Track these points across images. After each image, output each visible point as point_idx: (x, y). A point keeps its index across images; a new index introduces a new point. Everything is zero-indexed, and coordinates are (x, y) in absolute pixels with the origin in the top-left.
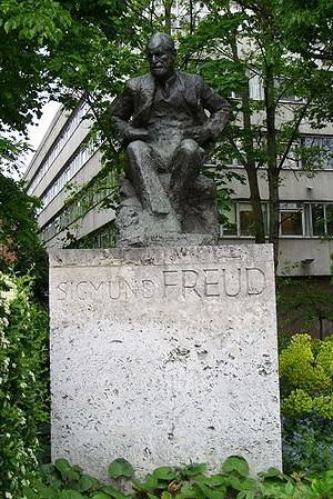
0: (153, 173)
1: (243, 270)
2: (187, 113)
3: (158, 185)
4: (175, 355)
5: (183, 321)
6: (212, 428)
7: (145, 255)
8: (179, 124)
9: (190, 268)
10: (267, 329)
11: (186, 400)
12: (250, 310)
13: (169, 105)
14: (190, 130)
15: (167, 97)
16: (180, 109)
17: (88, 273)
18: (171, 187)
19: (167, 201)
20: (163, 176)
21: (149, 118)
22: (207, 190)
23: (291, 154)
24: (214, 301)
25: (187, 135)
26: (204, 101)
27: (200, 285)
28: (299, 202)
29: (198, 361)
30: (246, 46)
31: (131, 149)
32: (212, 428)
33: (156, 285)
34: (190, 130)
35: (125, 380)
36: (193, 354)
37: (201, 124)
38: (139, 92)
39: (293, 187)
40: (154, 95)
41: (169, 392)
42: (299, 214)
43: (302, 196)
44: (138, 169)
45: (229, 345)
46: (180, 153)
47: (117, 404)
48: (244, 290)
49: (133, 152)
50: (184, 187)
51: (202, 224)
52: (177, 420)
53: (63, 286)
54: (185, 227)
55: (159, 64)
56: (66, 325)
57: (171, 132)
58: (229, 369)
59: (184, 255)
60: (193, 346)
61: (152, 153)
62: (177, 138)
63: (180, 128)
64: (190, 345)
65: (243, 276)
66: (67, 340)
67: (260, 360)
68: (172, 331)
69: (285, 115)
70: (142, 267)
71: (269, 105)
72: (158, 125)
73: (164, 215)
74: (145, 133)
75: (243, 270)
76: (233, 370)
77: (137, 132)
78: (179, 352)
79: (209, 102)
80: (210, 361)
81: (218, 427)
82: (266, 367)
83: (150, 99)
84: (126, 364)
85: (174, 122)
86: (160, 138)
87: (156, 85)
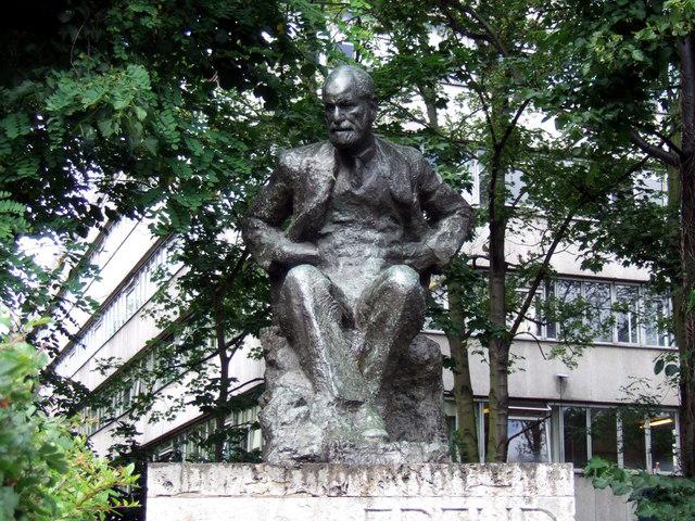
0: (334, 325)
1: (516, 511)
2: (393, 218)
8: (378, 236)
13: (361, 202)
14: (396, 248)
15: (358, 186)
16: (379, 209)
21: (323, 225)
22: (428, 362)
23: (532, 312)
25: (393, 259)
26: (424, 196)
30: (460, 108)
31: (293, 279)
34: (396, 248)
38: (305, 175)
39: (533, 373)
40: (333, 183)
43: (548, 390)
44: (306, 317)
46: (380, 293)
49: (297, 286)
50: (392, 356)
51: (417, 427)
54: (395, 434)
55: (345, 124)
57: (360, 253)
61: (334, 291)
62: (374, 263)
63: (380, 244)
69: (523, 243)
70: (324, 499)
71: (498, 219)
72: (339, 238)
79: (433, 199)
83: (324, 187)
85: (370, 234)
86: (342, 261)
87: (337, 162)
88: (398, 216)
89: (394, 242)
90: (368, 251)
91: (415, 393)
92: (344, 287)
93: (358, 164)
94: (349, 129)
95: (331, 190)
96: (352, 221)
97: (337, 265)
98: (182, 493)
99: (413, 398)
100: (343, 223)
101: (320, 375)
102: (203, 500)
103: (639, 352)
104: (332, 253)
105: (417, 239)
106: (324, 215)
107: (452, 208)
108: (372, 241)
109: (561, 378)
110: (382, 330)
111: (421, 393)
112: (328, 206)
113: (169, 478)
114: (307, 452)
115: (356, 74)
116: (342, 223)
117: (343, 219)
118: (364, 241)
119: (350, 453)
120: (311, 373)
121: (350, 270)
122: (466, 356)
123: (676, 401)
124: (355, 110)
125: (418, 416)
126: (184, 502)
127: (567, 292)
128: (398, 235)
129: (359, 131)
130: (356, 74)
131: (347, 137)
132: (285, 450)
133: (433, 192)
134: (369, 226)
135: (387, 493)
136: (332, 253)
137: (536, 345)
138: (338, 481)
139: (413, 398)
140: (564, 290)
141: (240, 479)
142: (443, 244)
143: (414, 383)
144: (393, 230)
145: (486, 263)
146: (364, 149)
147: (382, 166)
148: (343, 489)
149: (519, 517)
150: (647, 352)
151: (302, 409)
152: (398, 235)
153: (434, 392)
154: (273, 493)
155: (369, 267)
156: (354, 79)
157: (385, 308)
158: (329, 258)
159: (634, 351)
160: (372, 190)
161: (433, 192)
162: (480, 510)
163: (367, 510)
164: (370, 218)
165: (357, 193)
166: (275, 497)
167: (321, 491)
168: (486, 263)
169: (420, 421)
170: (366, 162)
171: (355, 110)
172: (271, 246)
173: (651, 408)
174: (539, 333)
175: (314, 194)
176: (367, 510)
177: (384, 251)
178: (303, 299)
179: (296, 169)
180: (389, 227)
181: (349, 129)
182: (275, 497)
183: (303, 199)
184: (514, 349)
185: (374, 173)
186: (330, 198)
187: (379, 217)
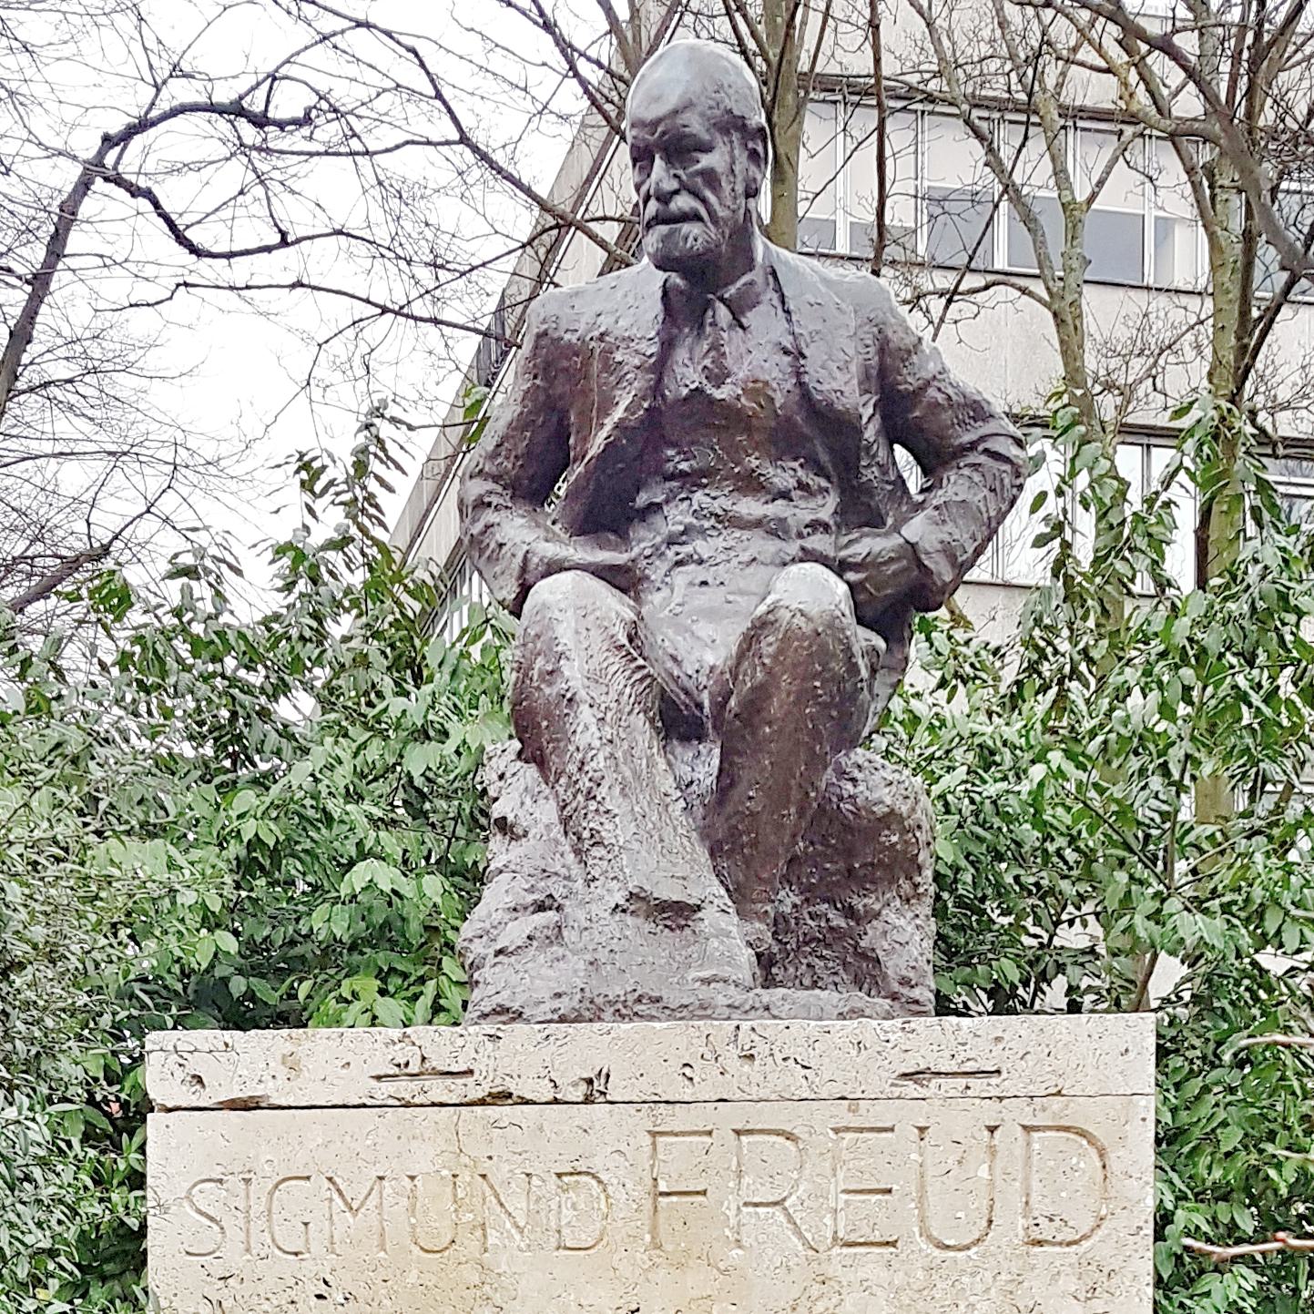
15: (719, 378)
20: (684, 753)
37: (874, 521)
40: (660, 366)
73: (677, 914)
83: (640, 383)
88: (824, 458)
91: (858, 903)
95: (657, 389)
99: (850, 912)
107: (967, 438)
128: (826, 508)
139: (850, 912)
165: (719, 394)
176: (654, 1134)
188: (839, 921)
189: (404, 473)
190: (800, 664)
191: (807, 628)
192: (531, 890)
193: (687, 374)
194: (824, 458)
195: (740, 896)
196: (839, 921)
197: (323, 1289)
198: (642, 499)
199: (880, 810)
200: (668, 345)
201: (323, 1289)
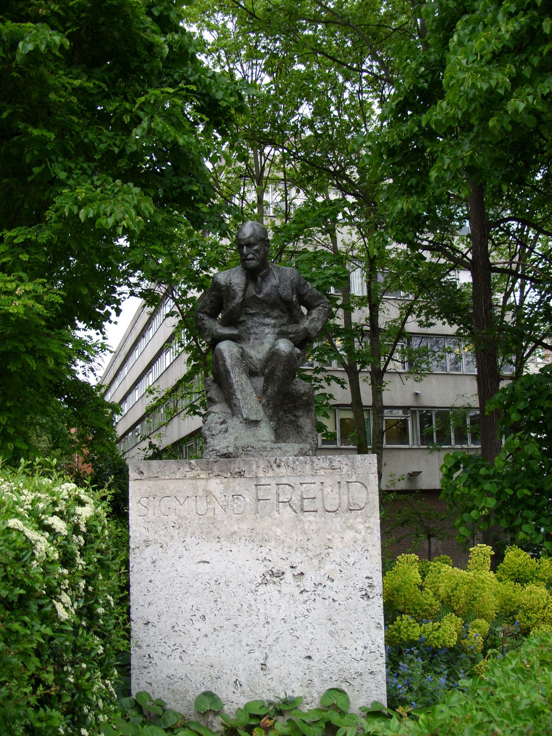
0: (244, 376)
1: (343, 483)
2: (282, 310)
3: (249, 389)
4: (268, 577)
5: (277, 538)
6: (309, 657)
7: (237, 465)
8: (273, 321)
9: (285, 481)
10: (370, 548)
11: (280, 626)
12: (351, 527)
13: (262, 302)
14: (284, 328)
15: (259, 293)
16: (273, 305)
17: (172, 486)
18: (264, 391)
19: (260, 407)
20: (255, 380)
21: (240, 316)
23: (397, 356)
24: (310, 517)
27: (296, 500)
28: (405, 409)
29: (294, 584)
31: (220, 350)
32: (309, 657)
33: (248, 500)
34: (284, 328)
35: (212, 604)
36: (289, 575)
38: (229, 287)
40: (245, 290)
41: (262, 617)
42: (405, 422)
43: (409, 401)
44: (227, 372)
45: (328, 567)
47: (204, 632)
48: (345, 505)
51: (298, 433)
52: (270, 650)
53: (144, 501)
55: (250, 256)
56: (147, 542)
58: (328, 593)
59: (279, 466)
60: (287, 567)
61: (243, 355)
62: (270, 338)
63: (274, 326)
64: (284, 566)
65: (344, 489)
66: (149, 561)
67: (362, 583)
68: (265, 550)
70: (231, 480)
72: (250, 323)
73: (255, 423)
74: (235, 332)
75: (343, 483)
76: (333, 594)
77: (226, 331)
78: (272, 574)
79: (306, 298)
80: (307, 583)
81: (316, 657)
82: (368, 589)
83: (240, 294)
84: (214, 587)
85: (268, 321)
86: (252, 337)
88: (285, 309)
89: (283, 325)
90: (267, 331)
92: (252, 353)
93: (259, 279)
94: (252, 259)
95: (244, 295)
96: (257, 313)
97: (249, 339)
98: (150, 478)
99: (295, 416)
100: (253, 315)
101: (236, 406)
102: (161, 481)
103: (462, 378)
104: (246, 332)
105: (297, 322)
106: (241, 310)
107: (318, 303)
108: (269, 325)
109: (417, 394)
110: (273, 377)
111: (300, 413)
112: (244, 304)
113: (142, 469)
114: (225, 451)
115: (256, 227)
116: (251, 314)
117: (251, 312)
118: (265, 325)
119: (250, 451)
120: (230, 404)
121: (257, 342)
122: (358, 383)
123: (478, 406)
124: (256, 248)
125: (299, 426)
126: (151, 483)
127: (421, 342)
128: (285, 320)
129: (258, 260)
130: (256, 227)
131: (253, 263)
132: (213, 451)
133: (306, 294)
134: (268, 316)
135: (268, 475)
136: (246, 332)
137: (397, 375)
138: (239, 469)
139: (295, 416)
140: (418, 342)
141: (181, 470)
142: (312, 325)
143: (295, 407)
144: (282, 317)
145: (368, 328)
146: (262, 271)
147: (274, 281)
148: (242, 473)
149: (346, 488)
150: (467, 377)
151: (223, 426)
152: (285, 320)
153: (308, 412)
154: (201, 476)
155: (268, 340)
156: (254, 230)
157: (274, 365)
158: (244, 335)
159: (459, 377)
160: (268, 295)
161: (306, 294)
162: (322, 483)
163: (256, 485)
164: (268, 311)
165: (259, 296)
166: (203, 479)
167: (229, 475)
168: (368, 328)
169: (299, 430)
170: (264, 278)
171: (256, 248)
172: (210, 329)
173: (470, 408)
174: (404, 368)
175: (234, 298)
176: (256, 485)
177: (277, 330)
178: (225, 361)
179: (223, 283)
180: (280, 316)
181: (252, 259)
182: (203, 479)
183: (228, 301)
184: (386, 378)
185: (270, 284)
186: (243, 300)
187: (273, 311)
188: (293, 419)
189: (208, 562)
190: (435, 672)
191: (285, 355)
192: (219, 418)
193: (252, 290)
194: (285, 309)
195: (271, 418)
196: (293, 419)
197: (174, 525)
198: (241, 319)
199: (302, 392)
200: (247, 285)
201: (174, 525)
